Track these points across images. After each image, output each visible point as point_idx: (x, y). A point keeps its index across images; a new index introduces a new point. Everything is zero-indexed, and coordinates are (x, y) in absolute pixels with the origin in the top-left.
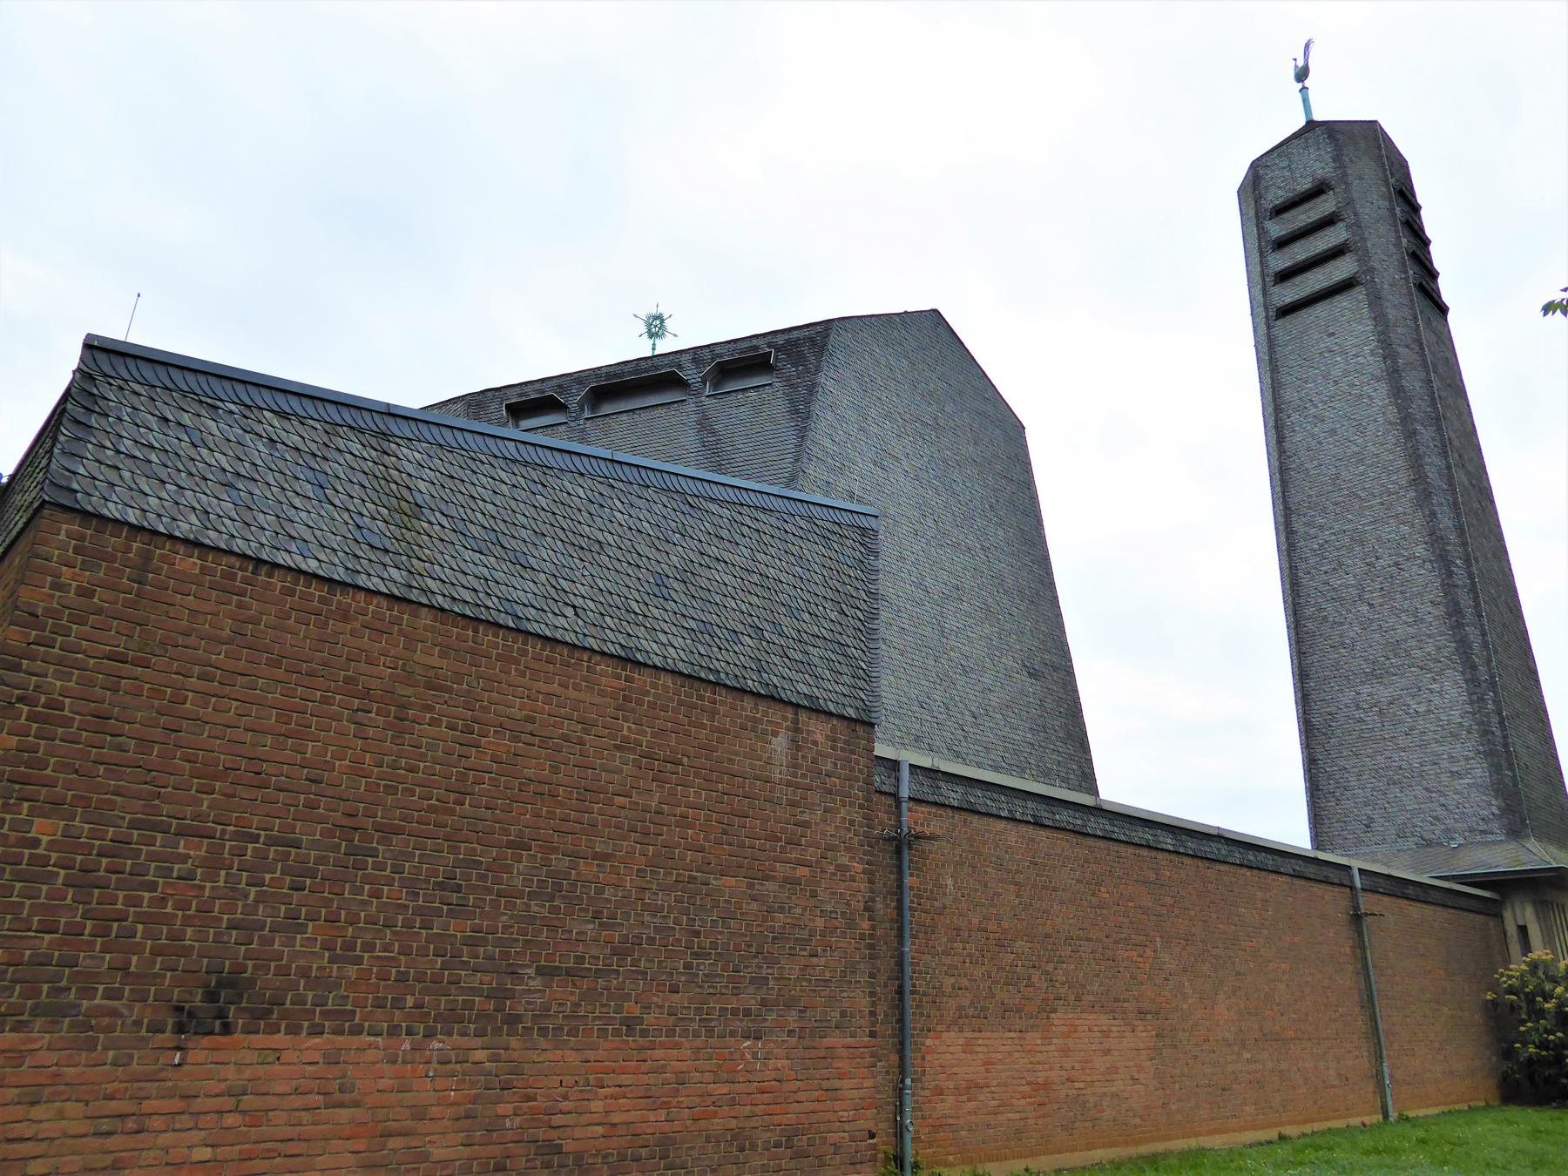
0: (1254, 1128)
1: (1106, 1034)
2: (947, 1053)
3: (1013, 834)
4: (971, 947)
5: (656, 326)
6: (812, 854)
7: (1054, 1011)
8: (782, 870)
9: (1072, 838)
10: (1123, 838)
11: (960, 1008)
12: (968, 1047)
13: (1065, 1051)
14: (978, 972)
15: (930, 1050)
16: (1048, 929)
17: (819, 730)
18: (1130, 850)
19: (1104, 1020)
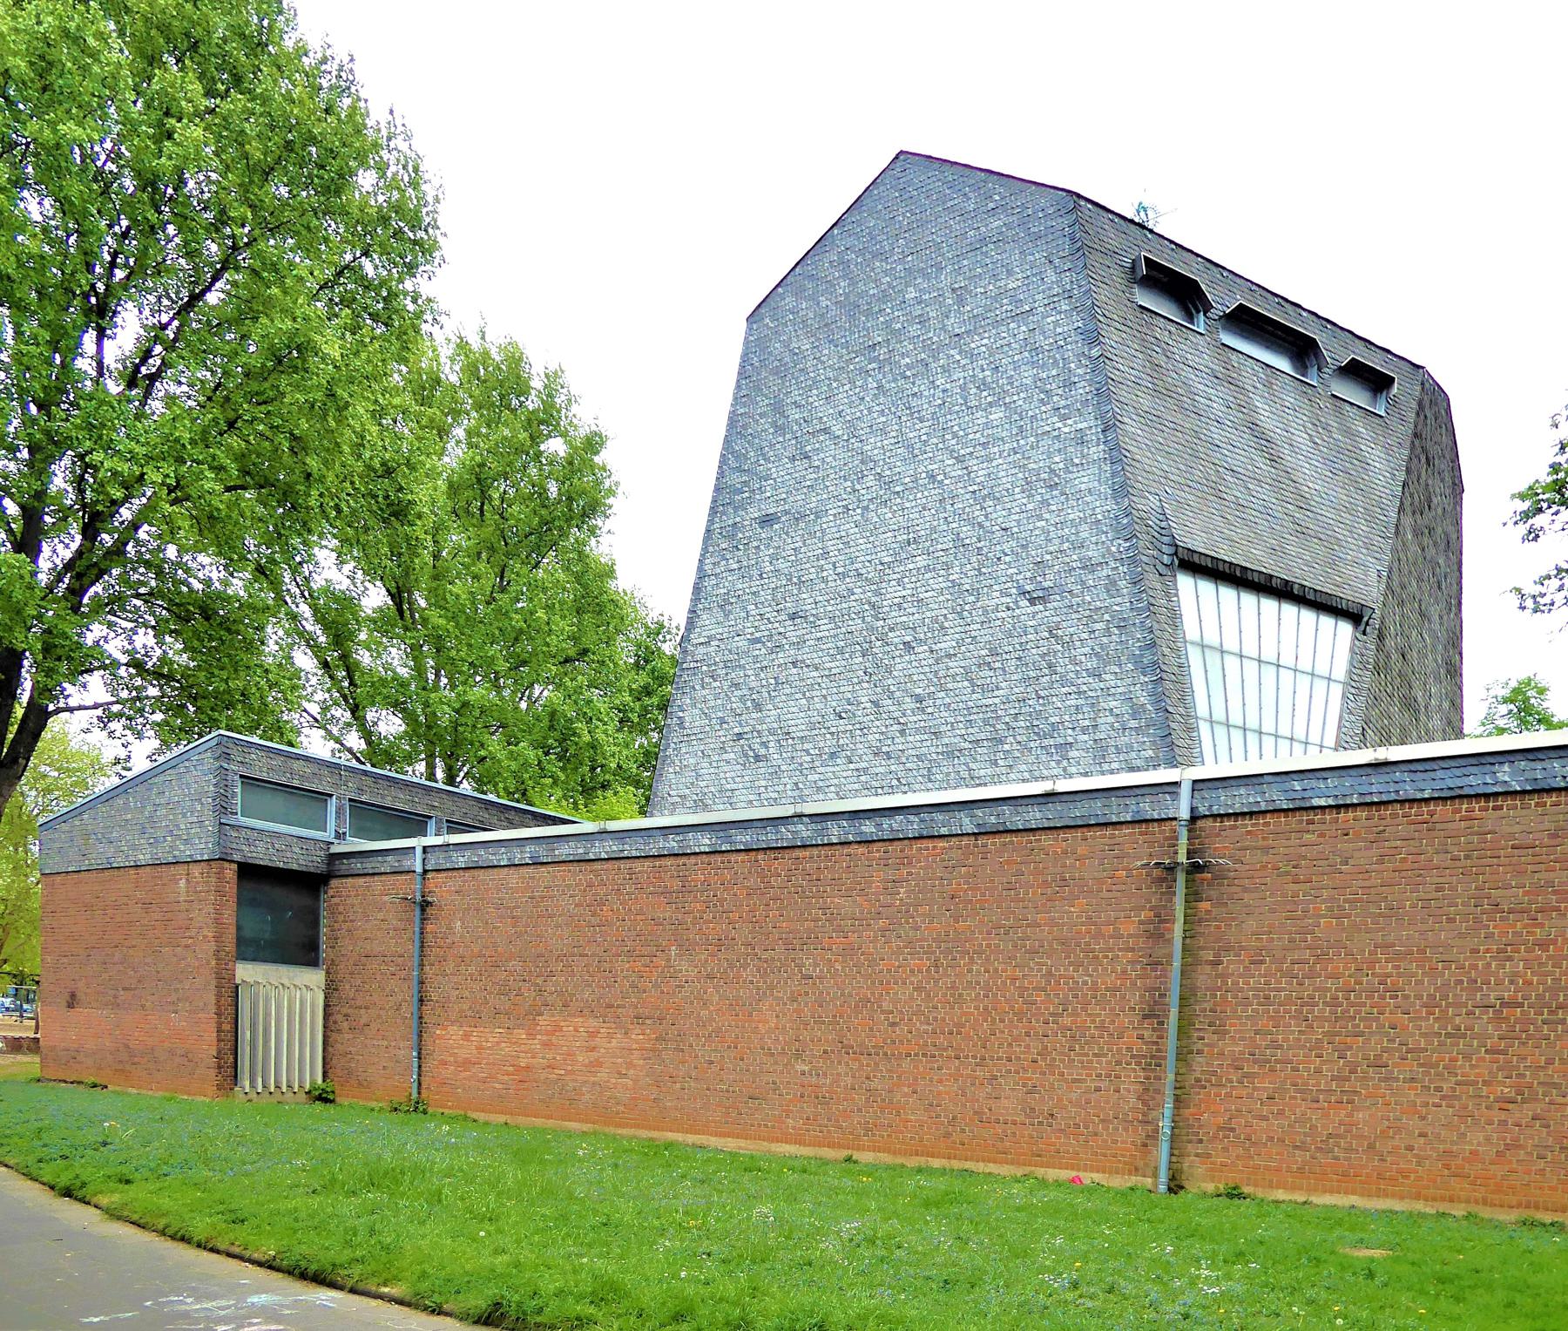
0: (800, 1142)
1: (593, 1034)
2: (450, 1039)
3: (513, 877)
4: (472, 969)
5: (1142, 208)
6: (193, 933)
7: (541, 1014)
8: (184, 942)
9: (575, 868)
10: (634, 853)
11: (461, 1011)
12: (466, 1037)
13: (546, 1045)
14: (476, 986)
15: (440, 1037)
16: (541, 949)
17: (196, 870)
18: (647, 863)
19: (593, 1023)
